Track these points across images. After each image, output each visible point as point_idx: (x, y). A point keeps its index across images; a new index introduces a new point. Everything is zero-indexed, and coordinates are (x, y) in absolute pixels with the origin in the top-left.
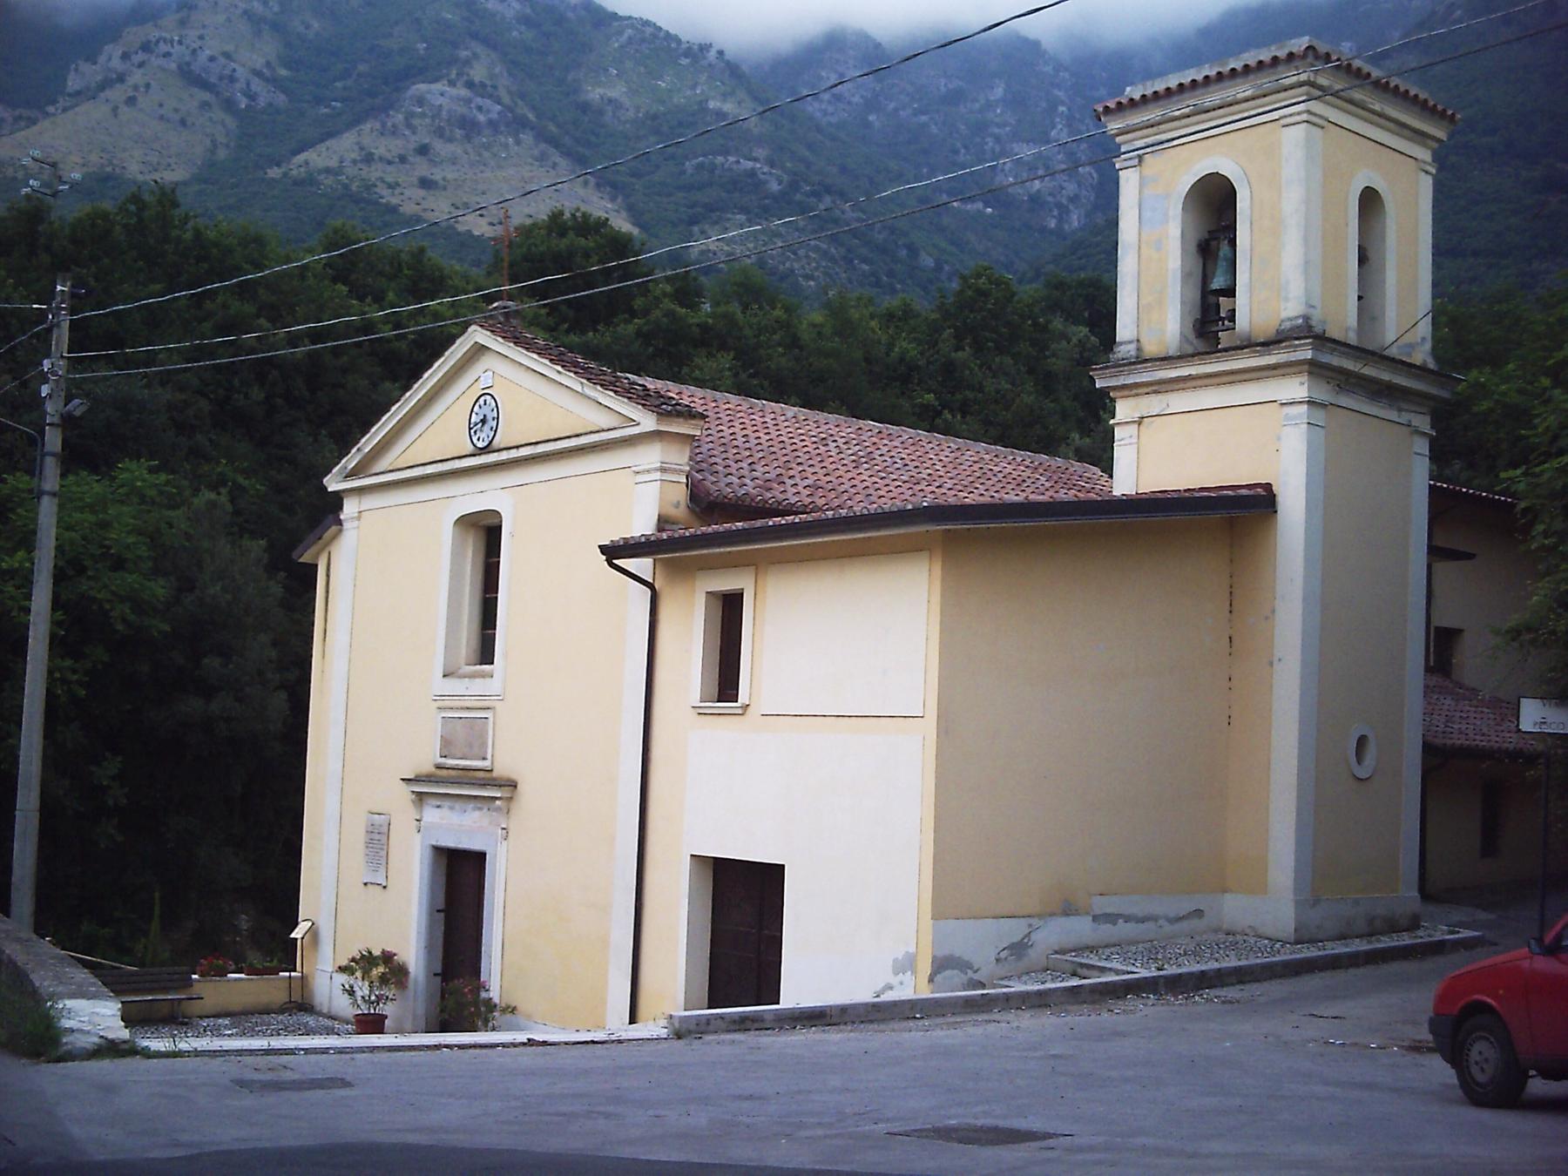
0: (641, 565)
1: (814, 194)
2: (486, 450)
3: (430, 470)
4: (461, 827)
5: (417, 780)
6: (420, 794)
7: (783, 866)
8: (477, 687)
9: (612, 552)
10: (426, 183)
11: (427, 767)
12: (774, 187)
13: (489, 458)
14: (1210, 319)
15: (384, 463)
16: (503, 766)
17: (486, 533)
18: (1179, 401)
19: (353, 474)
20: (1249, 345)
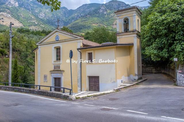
0: (79, 50)
1: (40, 24)
2: (57, 41)
3: (54, 42)
4: (57, 75)
5: (51, 71)
6: (52, 73)
7: (99, 76)
8: (58, 62)
9: (78, 49)
10: (3, 22)
11: (52, 70)
12: (37, 23)
13: (58, 41)
14: (126, 30)
15: (44, 42)
16: (61, 69)
17: (58, 49)
18: (123, 37)
19: (40, 43)
20: (130, 32)
